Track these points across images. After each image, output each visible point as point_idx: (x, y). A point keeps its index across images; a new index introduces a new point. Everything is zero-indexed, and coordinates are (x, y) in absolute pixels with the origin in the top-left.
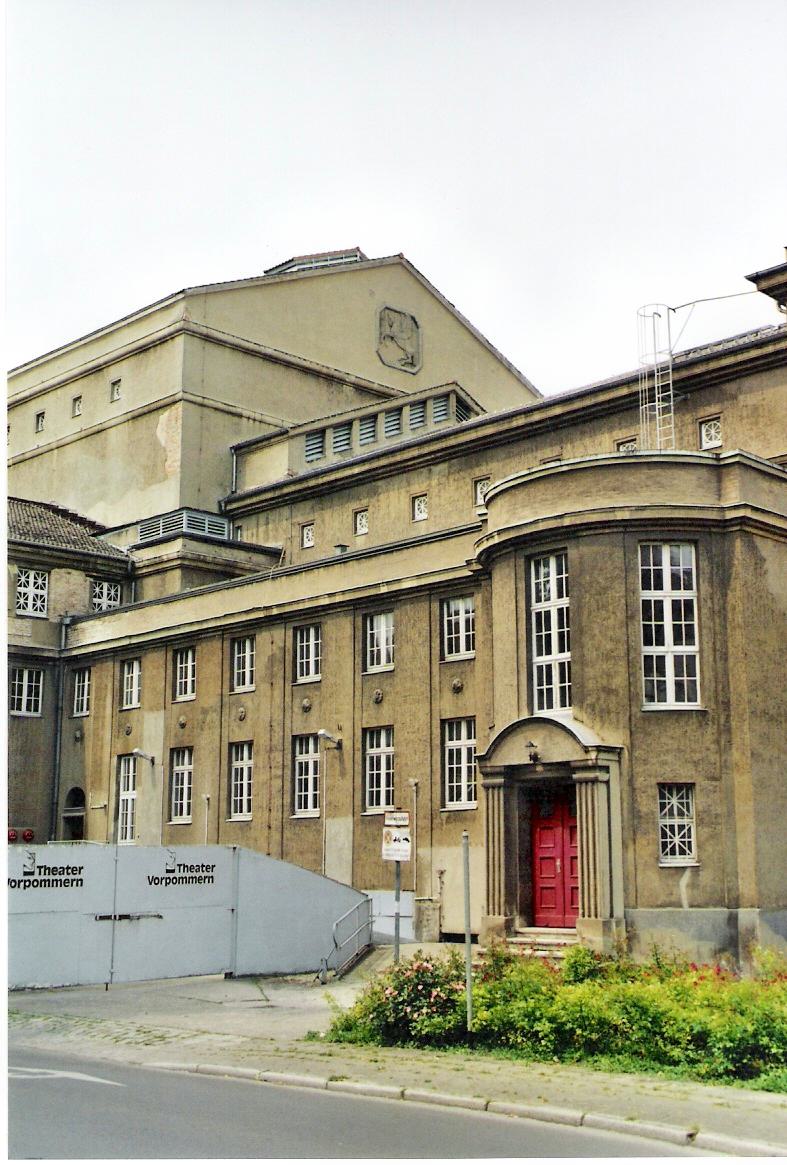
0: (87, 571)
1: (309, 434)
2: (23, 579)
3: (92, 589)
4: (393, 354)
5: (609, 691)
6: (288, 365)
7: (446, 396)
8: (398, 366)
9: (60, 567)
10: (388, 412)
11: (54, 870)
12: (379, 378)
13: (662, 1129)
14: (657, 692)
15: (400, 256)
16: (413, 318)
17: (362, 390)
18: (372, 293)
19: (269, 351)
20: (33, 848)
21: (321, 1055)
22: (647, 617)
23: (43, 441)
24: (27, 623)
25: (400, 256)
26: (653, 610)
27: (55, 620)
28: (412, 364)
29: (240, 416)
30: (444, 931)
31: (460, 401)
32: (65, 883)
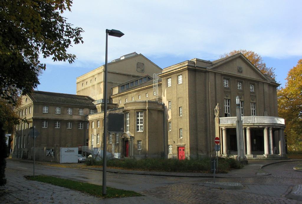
0: (89, 108)
1: (121, 86)
2: (80, 110)
3: (90, 111)
4: (139, 70)
5: (133, 130)
6: (121, 74)
7: (146, 77)
8: (140, 72)
9: (85, 108)
10: (140, 79)
11: (71, 150)
12: (136, 74)
13: (128, 171)
14: (138, 130)
15: (141, 54)
16: (143, 64)
17: (134, 76)
18: (135, 61)
19: (117, 73)
20: (68, 148)
21: (28, 178)
22: (137, 121)
23: (83, 88)
24: (80, 116)
25: (141, 54)
26: (138, 120)
27: (84, 116)
28: (143, 71)
29: (113, 83)
30: (78, 162)
31: (148, 78)
32: (72, 152)
